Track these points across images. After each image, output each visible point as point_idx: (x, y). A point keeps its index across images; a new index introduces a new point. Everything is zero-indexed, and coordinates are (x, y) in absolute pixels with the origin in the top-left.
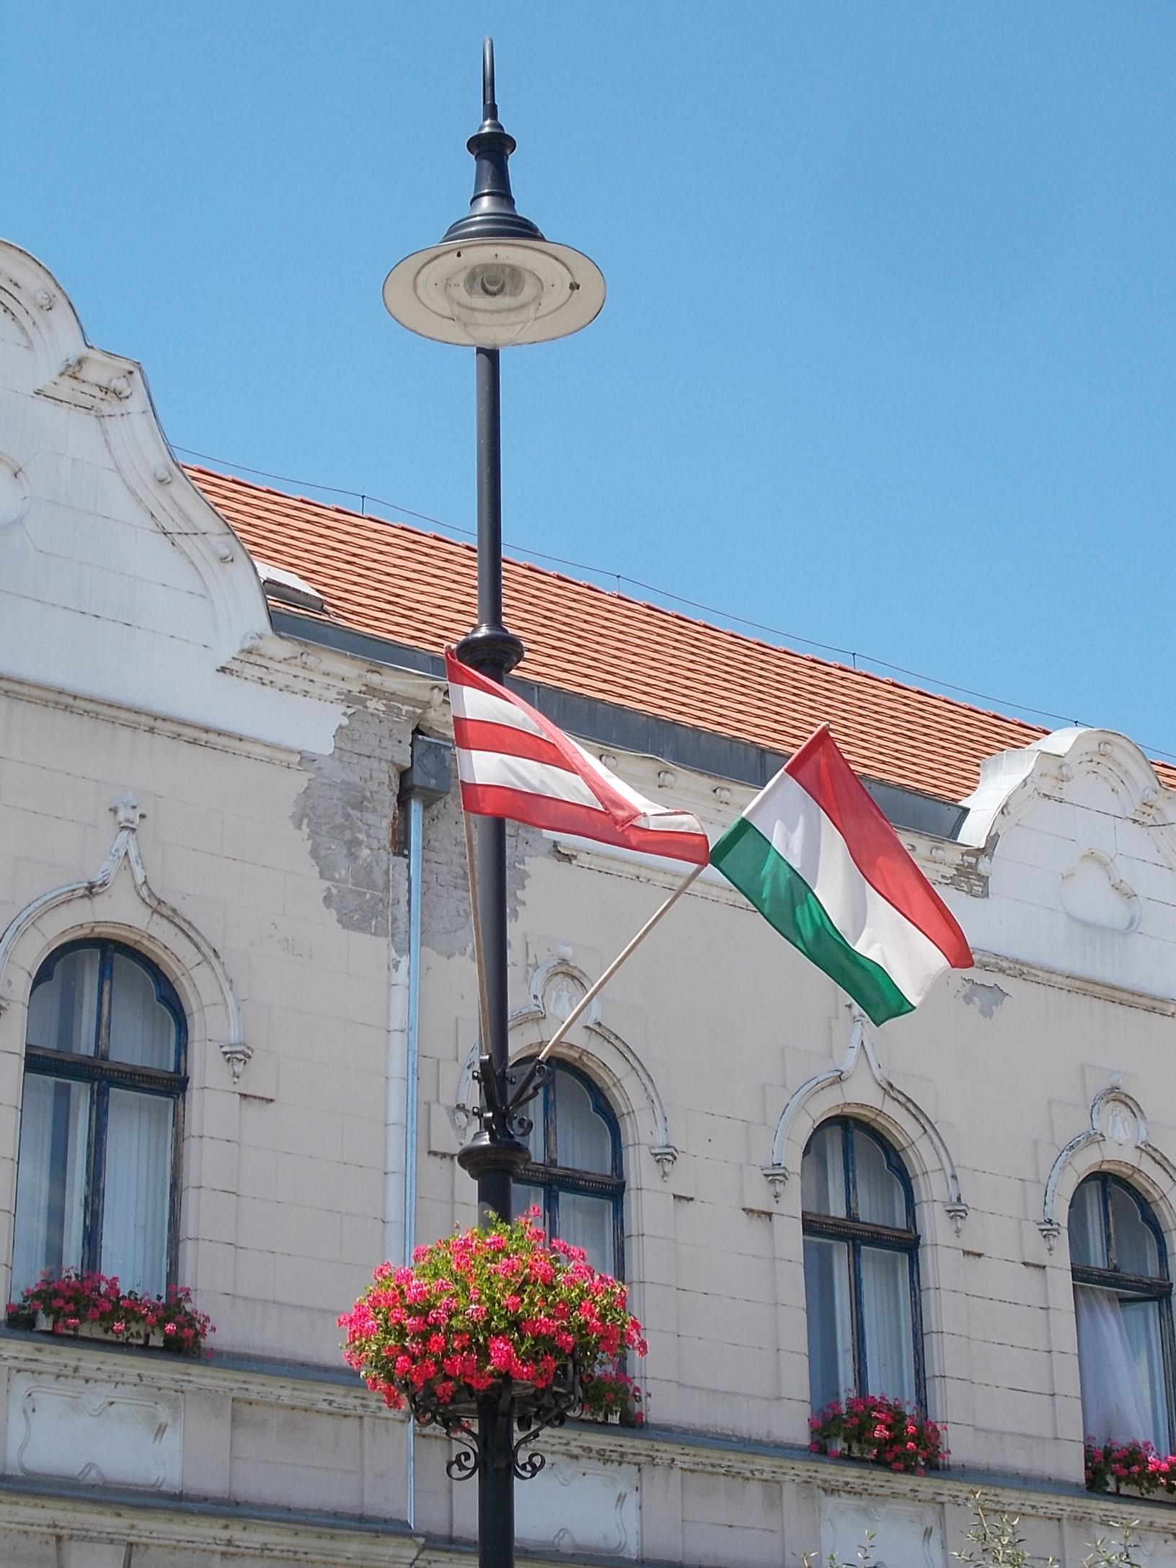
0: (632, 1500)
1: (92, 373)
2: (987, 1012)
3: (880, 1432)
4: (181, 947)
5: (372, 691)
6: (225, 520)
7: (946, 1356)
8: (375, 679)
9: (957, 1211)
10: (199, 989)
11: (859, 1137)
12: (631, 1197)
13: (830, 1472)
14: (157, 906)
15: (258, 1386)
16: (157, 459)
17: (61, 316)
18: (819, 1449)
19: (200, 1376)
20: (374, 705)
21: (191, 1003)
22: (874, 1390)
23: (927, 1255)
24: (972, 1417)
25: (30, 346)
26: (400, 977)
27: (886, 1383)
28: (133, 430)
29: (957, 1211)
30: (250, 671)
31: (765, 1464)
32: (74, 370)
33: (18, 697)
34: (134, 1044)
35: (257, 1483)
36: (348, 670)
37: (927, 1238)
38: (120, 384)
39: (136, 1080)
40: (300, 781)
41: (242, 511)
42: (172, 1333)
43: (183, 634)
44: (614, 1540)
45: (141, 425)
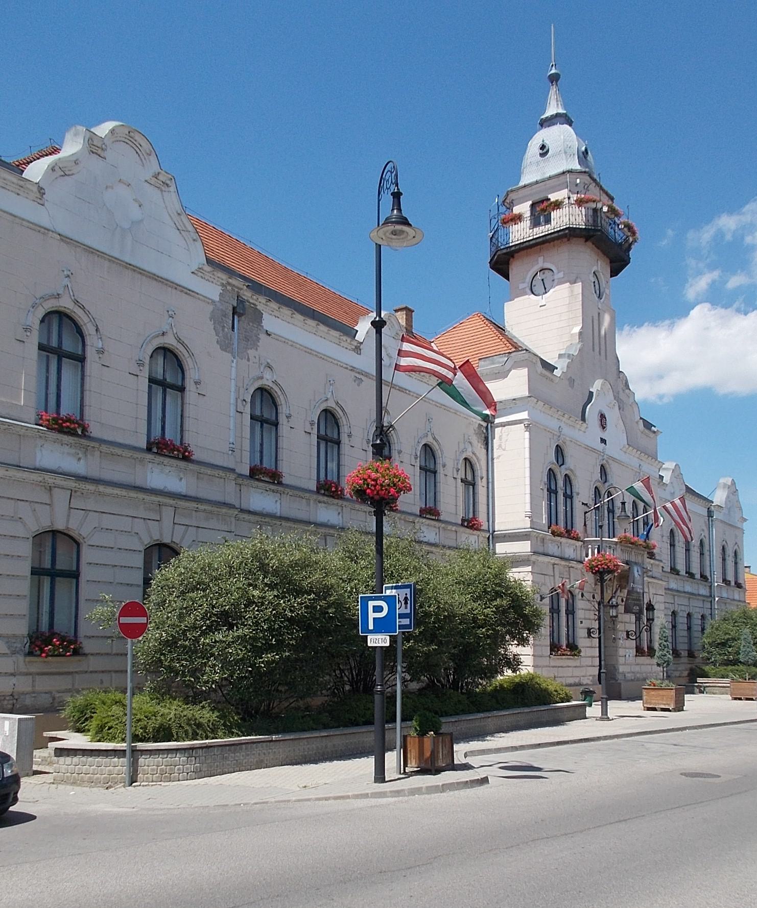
0: (278, 503)
1: (161, 177)
2: (358, 385)
3: (333, 489)
4: (184, 352)
5: (229, 284)
6: (196, 229)
7: (283, 455)
8: (230, 280)
9: (350, 436)
10: (188, 363)
11: (265, 394)
12: (280, 427)
13: (321, 498)
14: (179, 340)
15: (203, 469)
16: (178, 207)
17: (153, 158)
18: (149, 449)
19: (191, 466)
20: (229, 288)
21: (186, 367)
22: (167, 437)
23: (342, 446)
24: (99, 420)
25: (143, 165)
26: (234, 365)
27: (332, 477)
28: (171, 197)
29: (400, 452)
30: (200, 274)
31: (307, 495)
32: (156, 176)
33: (143, 275)
34: (68, 345)
35: (202, 494)
36: (224, 276)
37: (342, 442)
38: (168, 182)
39: (72, 357)
40: (211, 308)
41: (201, 230)
42: (184, 455)
43: (183, 262)
44: (275, 511)
45: (174, 196)
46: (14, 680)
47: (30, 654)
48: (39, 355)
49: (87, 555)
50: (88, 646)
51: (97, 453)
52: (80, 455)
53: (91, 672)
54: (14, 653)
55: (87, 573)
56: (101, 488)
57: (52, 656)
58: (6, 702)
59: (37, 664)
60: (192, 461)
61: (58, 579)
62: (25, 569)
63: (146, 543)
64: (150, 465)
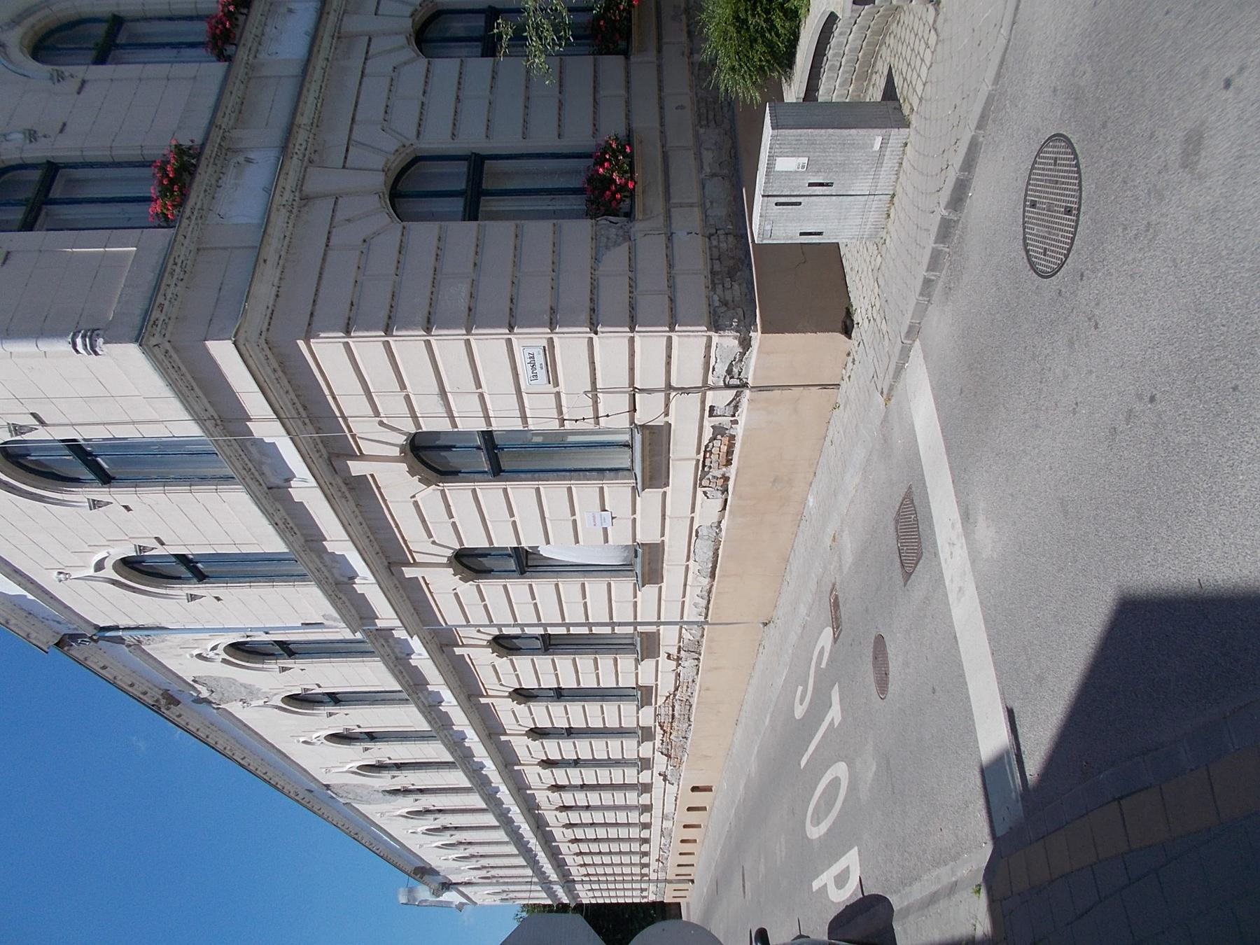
7: (127, 148)
46: (681, 236)
47: (629, 215)
48: (118, 62)
49: (437, 139)
50: (613, 127)
51: (236, 133)
52: (241, 159)
53: (662, 125)
54: (628, 237)
55: (473, 139)
56: (304, 119)
57: (632, 171)
58: (723, 246)
59: (649, 201)
60: (203, 145)
61: (484, 186)
62: (464, 231)
63: (413, 54)
64: (262, 56)
